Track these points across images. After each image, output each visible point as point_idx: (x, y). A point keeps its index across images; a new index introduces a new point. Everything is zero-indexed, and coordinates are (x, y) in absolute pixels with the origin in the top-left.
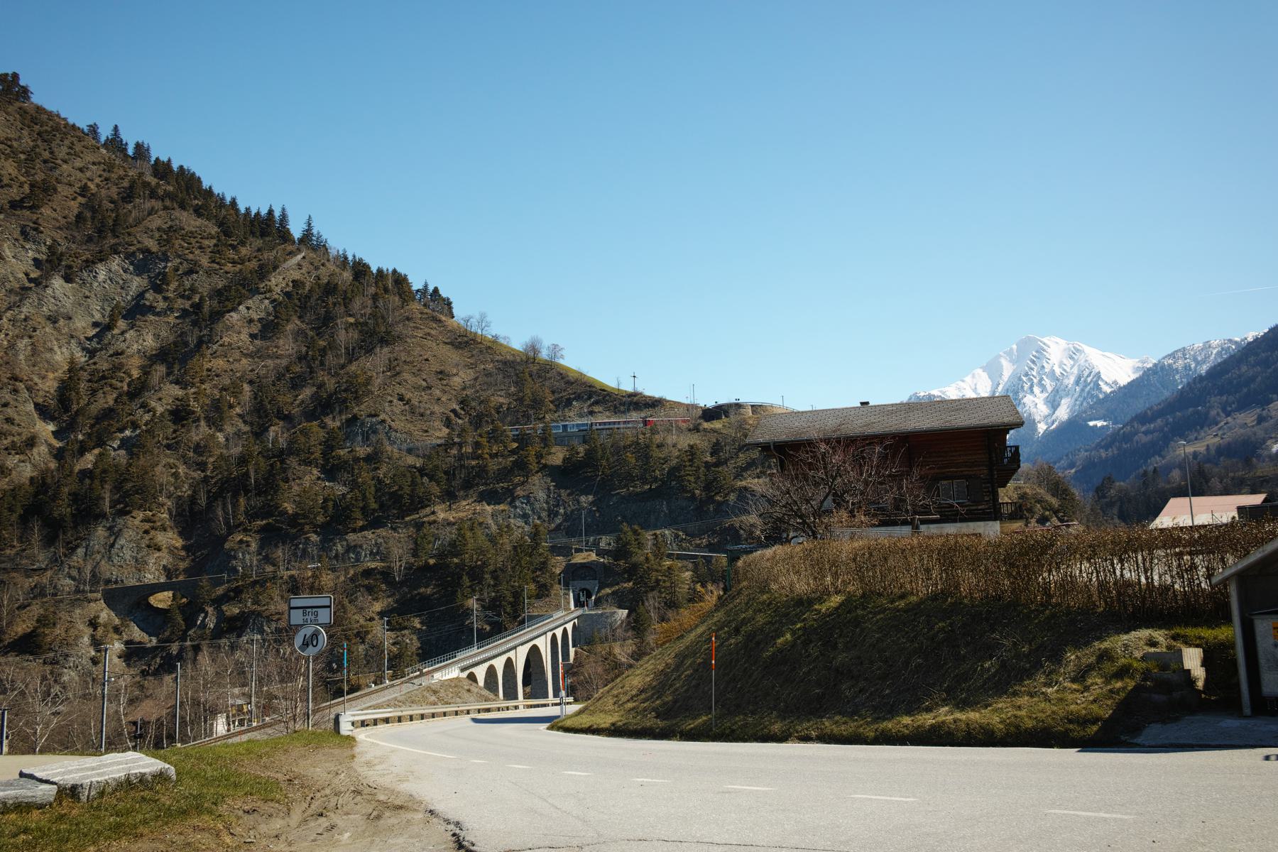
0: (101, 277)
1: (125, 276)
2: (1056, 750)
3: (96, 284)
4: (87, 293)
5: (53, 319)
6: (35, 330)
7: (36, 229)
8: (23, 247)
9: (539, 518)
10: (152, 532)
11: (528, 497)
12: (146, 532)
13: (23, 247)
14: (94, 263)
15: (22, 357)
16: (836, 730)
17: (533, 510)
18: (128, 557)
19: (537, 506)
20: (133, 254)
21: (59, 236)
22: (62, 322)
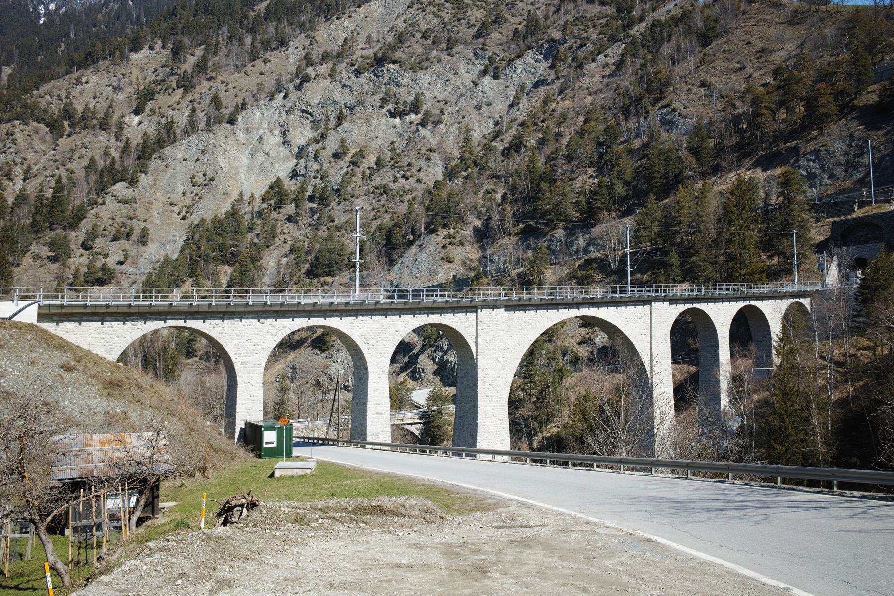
0: (518, 70)
1: (536, 65)
2: (480, 422)
3: (514, 76)
4: (508, 84)
5: (478, 108)
6: (464, 117)
7: (482, 49)
8: (474, 63)
9: (831, 177)
10: (450, 247)
11: (817, 153)
12: (444, 247)
13: (474, 63)
14: (513, 60)
15: (451, 138)
16: (752, 291)
17: (822, 168)
18: (424, 269)
19: (830, 161)
20: (542, 45)
21: (497, 50)
22: (484, 108)
